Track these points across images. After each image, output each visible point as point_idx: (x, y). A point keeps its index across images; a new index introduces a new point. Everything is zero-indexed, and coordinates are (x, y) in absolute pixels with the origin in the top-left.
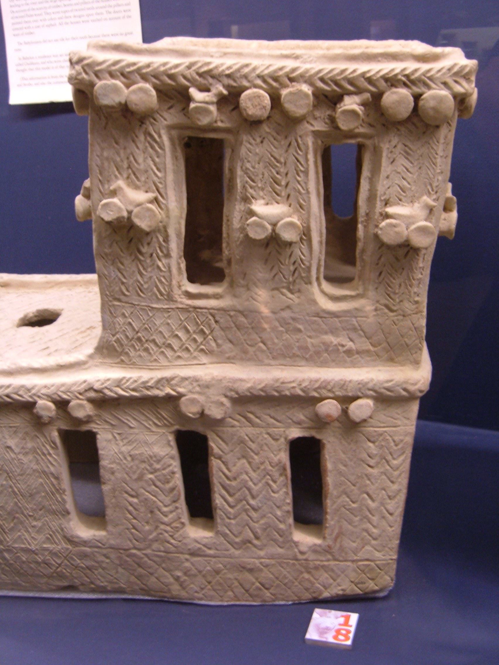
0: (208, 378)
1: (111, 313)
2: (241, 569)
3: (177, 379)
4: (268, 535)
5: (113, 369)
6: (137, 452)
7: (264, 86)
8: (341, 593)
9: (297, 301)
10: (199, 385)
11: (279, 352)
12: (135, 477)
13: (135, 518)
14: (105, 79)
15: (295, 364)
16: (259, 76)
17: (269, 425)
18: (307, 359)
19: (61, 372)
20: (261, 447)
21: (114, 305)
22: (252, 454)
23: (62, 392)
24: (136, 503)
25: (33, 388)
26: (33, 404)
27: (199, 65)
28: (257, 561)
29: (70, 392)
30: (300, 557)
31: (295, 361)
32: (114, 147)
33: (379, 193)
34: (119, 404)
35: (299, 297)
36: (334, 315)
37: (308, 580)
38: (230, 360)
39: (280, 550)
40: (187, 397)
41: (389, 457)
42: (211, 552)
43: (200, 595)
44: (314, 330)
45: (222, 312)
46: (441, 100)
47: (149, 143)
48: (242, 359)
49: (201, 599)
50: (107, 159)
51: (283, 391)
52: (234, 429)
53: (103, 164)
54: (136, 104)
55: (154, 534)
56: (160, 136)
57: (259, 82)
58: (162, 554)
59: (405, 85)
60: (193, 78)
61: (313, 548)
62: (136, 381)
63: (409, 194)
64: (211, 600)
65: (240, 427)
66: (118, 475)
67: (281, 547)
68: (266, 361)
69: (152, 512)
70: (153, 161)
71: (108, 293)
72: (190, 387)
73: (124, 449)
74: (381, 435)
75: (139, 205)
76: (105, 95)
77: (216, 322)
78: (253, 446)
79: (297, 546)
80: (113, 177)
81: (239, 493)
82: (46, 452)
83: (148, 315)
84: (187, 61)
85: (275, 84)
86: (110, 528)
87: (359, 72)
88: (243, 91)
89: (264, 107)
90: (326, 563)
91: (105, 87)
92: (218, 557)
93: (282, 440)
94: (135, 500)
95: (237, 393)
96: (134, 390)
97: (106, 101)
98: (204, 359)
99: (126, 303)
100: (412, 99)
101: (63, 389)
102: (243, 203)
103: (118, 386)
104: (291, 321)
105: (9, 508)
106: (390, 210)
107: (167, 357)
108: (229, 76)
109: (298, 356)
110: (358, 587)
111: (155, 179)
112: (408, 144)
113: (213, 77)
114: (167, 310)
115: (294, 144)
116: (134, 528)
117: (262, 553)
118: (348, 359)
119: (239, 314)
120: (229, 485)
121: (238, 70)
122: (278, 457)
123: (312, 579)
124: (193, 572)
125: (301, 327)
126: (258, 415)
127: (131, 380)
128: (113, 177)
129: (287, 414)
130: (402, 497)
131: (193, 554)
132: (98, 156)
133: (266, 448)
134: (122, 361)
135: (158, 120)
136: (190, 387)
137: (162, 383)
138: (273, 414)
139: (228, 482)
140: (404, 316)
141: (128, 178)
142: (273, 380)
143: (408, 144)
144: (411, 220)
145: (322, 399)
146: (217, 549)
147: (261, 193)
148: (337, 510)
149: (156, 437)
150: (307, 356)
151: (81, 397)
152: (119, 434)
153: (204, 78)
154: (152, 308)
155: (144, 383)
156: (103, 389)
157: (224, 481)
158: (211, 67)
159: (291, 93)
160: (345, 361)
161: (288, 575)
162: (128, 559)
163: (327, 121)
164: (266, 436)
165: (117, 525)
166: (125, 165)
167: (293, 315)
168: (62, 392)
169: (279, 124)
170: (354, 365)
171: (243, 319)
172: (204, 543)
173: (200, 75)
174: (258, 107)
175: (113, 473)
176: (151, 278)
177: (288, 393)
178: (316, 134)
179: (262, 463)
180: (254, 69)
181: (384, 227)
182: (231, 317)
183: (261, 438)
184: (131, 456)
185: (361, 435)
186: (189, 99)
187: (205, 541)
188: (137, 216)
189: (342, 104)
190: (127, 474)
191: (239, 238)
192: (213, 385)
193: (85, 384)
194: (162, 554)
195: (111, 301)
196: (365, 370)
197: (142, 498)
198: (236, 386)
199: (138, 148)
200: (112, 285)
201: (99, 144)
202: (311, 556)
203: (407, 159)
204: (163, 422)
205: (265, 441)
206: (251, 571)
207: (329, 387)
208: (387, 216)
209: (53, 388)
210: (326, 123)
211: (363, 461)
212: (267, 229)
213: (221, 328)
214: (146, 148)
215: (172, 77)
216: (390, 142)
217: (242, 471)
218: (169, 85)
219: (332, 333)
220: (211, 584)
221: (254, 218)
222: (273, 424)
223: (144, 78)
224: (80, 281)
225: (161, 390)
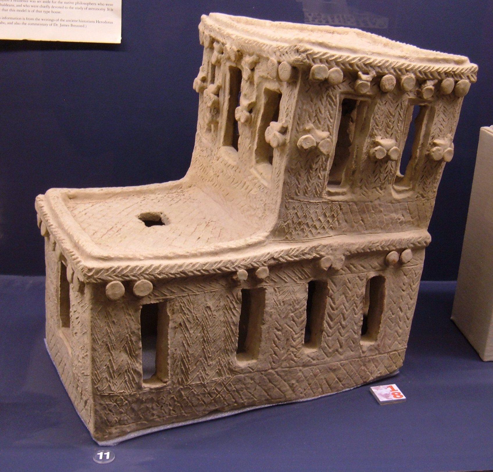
0: (336, 244)
1: (286, 207)
2: (329, 370)
3: (320, 247)
4: (348, 344)
5: (281, 244)
6: (287, 299)
7: (394, 74)
8: (379, 375)
9: (383, 194)
10: (332, 250)
11: (370, 225)
12: (283, 316)
13: (277, 346)
14: (318, 63)
15: (376, 232)
16: (393, 68)
17: (360, 271)
18: (382, 229)
19: (249, 250)
20: (354, 285)
21: (289, 202)
22: (349, 291)
23: (254, 262)
24: (280, 335)
25: (236, 262)
26: (235, 273)
27: (365, 59)
28: (339, 363)
29: (259, 262)
30: (362, 355)
31: (377, 230)
32: (310, 104)
33: (431, 132)
34: (281, 268)
35: (384, 192)
36: (398, 201)
37: (364, 371)
38: (344, 233)
39: (352, 353)
40: (325, 258)
41: (412, 284)
42: (314, 362)
43: (303, 395)
44: (388, 211)
45: (346, 203)
46: (466, 84)
47: (329, 102)
48: (350, 232)
49: (302, 398)
50: (305, 110)
51: (372, 249)
52: (342, 276)
53: (302, 113)
54: (333, 80)
55: (286, 355)
56: (336, 98)
57: (392, 71)
58: (287, 369)
59: (453, 77)
60: (362, 67)
61: (369, 348)
62: (298, 250)
63: (443, 133)
64: (308, 397)
65: (345, 274)
66: (274, 316)
67: (352, 351)
68: (363, 232)
69: (288, 340)
70: (329, 112)
71: (287, 194)
72: (327, 251)
73: (280, 298)
74: (410, 270)
75: (323, 139)
76: (319, 73)
77: (341, 209)
78: (350, 285)
79: (361, 348)
80: (306, 121)
81: (337, 318)
82: (232, 307)
83: (307, 207)
84: (359, 56)
85: (399, 73)
86: (260, 357)
87: (435, 69)
88: (383, 76)
89: (393, 85)
90: (374, 357)
91: (319, 68)
92: (318, 365)
93: (365, 280)
94: (280, 333)
95: (350, 252)
96: (296, 256)
97: (318, 77)
98: (331, 233)
99: (296, 200)
100: (454, 83)
101: (255, 260)
102: (369, 138)
103: (287, 255)
104: (378, 207)
105: (197, 354)
106: (436, 141)
107: (312, 234)
108: (379, 67)
109: (378, 227)
110: (387, 370)
111: (329, 123)
112: (446, 106)
113: (371, 67)
114: (317, 204)
115: (400, 105)
116: (275, 353)
117: (342, 357)
118: (400, 227)
119: (354, 204)
120: (333, 314)
121: (384, 64)
122: (361, 291)
123: (366, 369)
124: (302, 379)
125: (382, 209)
126: (355, 266)
127: (295, 250)
128: (306, 121)
129: (370, 263)
130: (413, 308)
131: (304, 366)
132: (299, 108)
133: (356, 286)
134: (287, 238)
135: (336, 88)
136: (327, 251)
137: (312, 250)
138: (363, 264)
139: (332, 312)
140: (428, 200)
141: (314, 122)
142: (368, 242)
143: (446, 106)
144: (446, 147)
145: (390, 252)
146: (318, 360)
147: (380, 133)
148: (385, 320)
149: (299, 287)
150: (382, 227)
151: (265, 264)
152: (278, 288)
153: (367, 67)
154: (310, 202)
155: (302, 251)
156: (279, 257)
157: (330, 311)
158: (371, 61)
159: (407, 79)
160: (399, 228)
161: (354, 369)
162: (265, 378)
163: (415, 93)
164: (357, 278)
165: (265, 353)
166: (314, 115)
167: (380, 203)
168: (254, 262)
169: (395, 94)
170: (402, 230)
171: (355, 207)
172: (312, 356)
173: (366, 65)
174: (391, 85)
175: (271, 316)
176: (313, 183)
177: (375, 250)
178: (410, 100)
179: (353, 296)
180: (391, 64)
181: (435, 151)
182: (349, 205)
183: (355, 280)
184: (283, 302)
185: (402, 272)
186: (357, 77)
187: (313, 355)
188: (322, 146)
189: (426, 85)
190: (279, 315)
191: (364, 158)
192: (338, 249)
193: (269, 255)
194: (287, 369)
195: (287, 200)
196: (407, 232)
197: (284, 331)
198: (350, 248)
199: (322, 104)
200: (291, 189)
201: (301, 101)
202: (368, 354)
203: (444, 114)
204: (304, 276)
205: (356, 282)
206: (334, 370)
207: (394, 244)
208: (435, 145)
209: (248, 260)
210: (415, 95)
211: (401, 287)
212: (385, 153)
213: (343, 213)
214: (326, 105)
215: (351, 65)
216: (439, 105)
217: (341, 303)
218: (349, 69)
219: (395, 212)
220: (311, 385)
221: (379, 147)
222: (362, 270)
223: (337, 64)
224: (133, 192)
225: (311, 255)
